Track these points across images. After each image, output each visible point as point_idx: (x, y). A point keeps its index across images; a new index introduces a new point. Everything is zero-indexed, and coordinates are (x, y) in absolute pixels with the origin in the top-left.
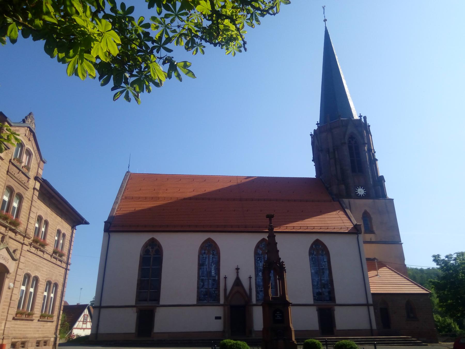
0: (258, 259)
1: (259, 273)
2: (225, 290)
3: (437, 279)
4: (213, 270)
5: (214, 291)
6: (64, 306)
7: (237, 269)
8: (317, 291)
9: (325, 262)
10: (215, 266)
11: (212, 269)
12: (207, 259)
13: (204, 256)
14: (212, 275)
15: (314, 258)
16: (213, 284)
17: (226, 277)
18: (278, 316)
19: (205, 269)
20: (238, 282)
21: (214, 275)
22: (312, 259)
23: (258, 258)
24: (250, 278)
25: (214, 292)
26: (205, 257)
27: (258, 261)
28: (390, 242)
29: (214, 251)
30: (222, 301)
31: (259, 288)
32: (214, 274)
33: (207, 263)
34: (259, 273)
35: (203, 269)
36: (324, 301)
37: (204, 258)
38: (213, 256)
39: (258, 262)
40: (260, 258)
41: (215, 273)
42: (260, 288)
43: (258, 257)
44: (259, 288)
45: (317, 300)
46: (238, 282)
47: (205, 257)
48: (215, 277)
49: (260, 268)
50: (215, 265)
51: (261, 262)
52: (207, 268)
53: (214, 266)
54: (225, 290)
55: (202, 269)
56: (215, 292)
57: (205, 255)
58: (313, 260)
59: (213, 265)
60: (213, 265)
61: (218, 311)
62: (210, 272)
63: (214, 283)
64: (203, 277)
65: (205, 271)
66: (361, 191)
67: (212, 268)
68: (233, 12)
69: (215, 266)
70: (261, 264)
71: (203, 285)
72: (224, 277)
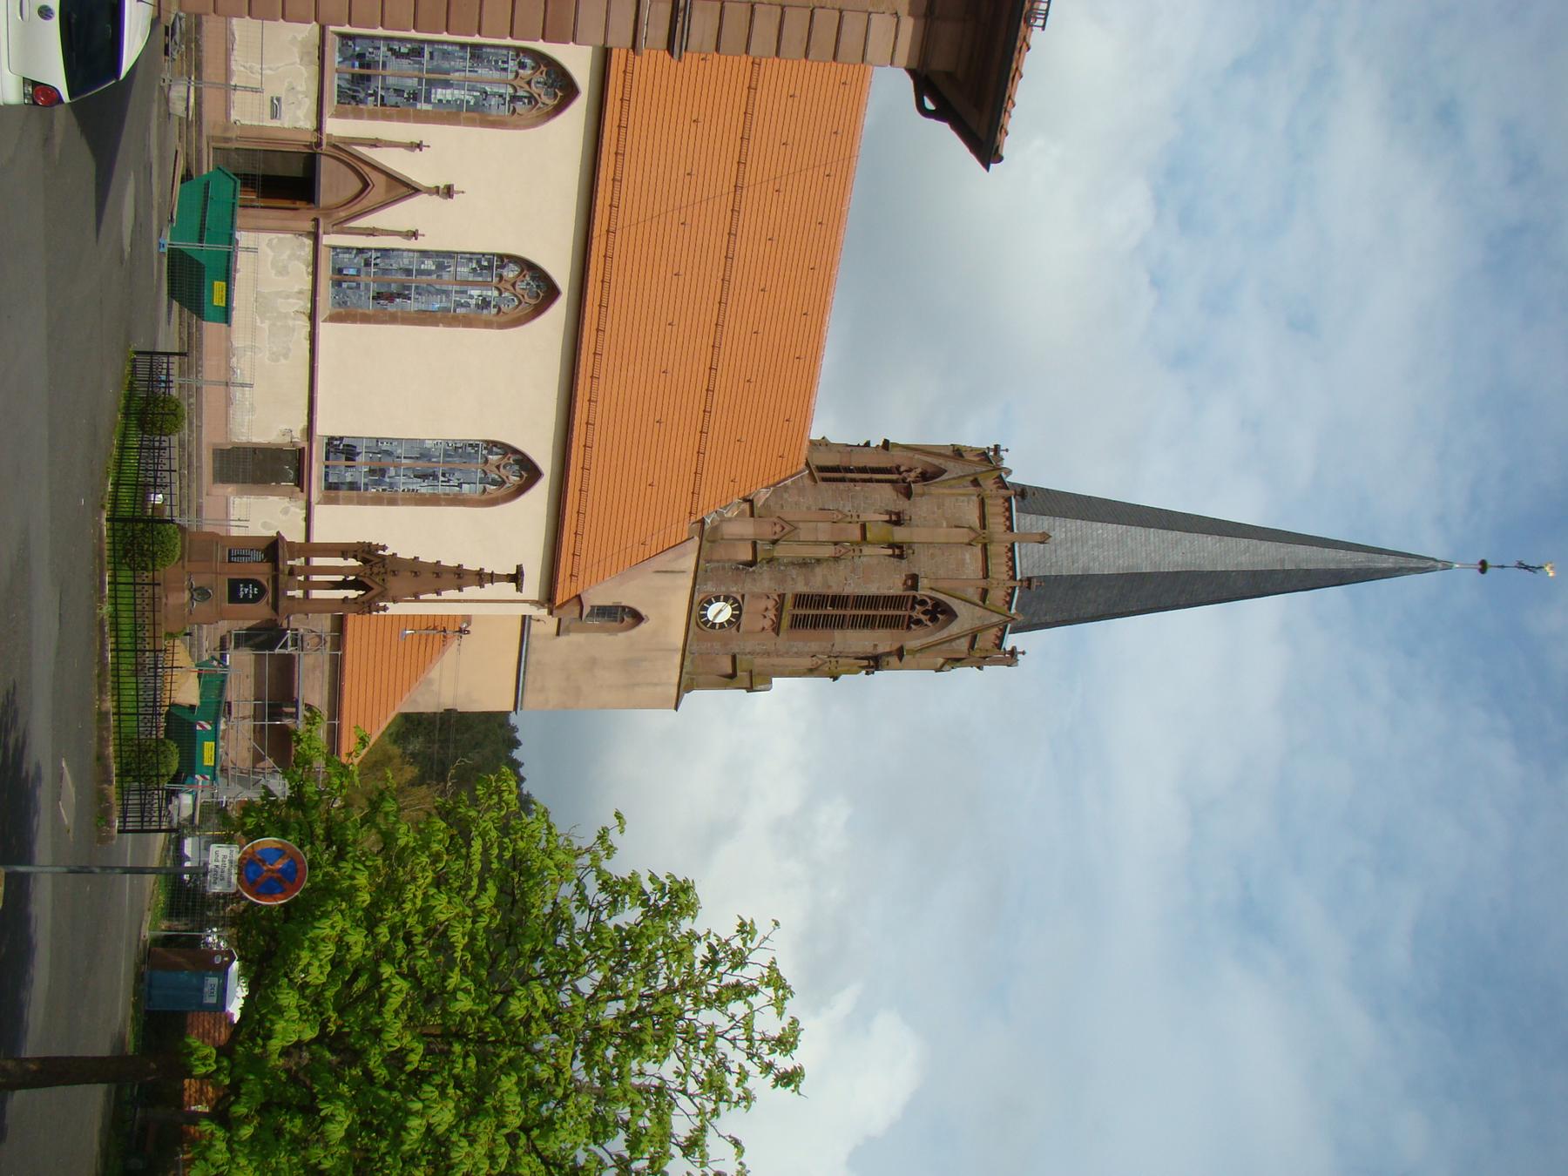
0: (486, 264)
1: (430, 262)
2: (375, 143)
3: (399, 784)
4: (453, 94)
5: (375, 94)
6: (202, 805)
7: (448, 192)
8: (361, 448)
9: (460, 485)
10: (468, 102)
11: (456, 92)
12: (496, 75)
13: (511, 63)
14: (433, 91)
15: (477, 452)
16: (399, 92)
17: (424, 149)
18: (246, 590)
19: (459, 64)
20: (404, 189)
21: (433, 96)
22: (471, 445)
23: (489, 262)
24: (415, 234)
25: (370, 92)
26: (506, 66)
27: (479, 262)
28: (524, 678)
29: (526, 101)
30: (336, 127)
31: (378, 258)
32: (439, 97)
33: (483, 72)
34: (430, 262)
35: (461, 58)
36: (327, 467)
37: (504, 62)
38: (508, 99)
39: (474, 261)
40: (490, 268)
41: (440, 101)
42: (378, 261)
43: (489, 261)
44: (378, 258)
45: (328, 444)
46: (404, 189)
47: (506, 66)
48: (428, 100)
49: (450, 266)
50: (472, 103)
51: (474, 270)
52: (463, 74)
53: (467, 97)
54: (375, 143)
55: (461, 54)
56: (372, 99)
57: (514, 69)
58: (469, 449)
59: (475, 94)
60: (475, 94)
61: (297, 118)
62: (447, 84)
63: (406, 95)
64: (431, 54)
65: (453, 63)
66: (720, 612)
67: (463, 92)
68: (701, 1121)
69: (468, 102)
70: (466, 270)
71: (398, 55)
72: (421, 142)
